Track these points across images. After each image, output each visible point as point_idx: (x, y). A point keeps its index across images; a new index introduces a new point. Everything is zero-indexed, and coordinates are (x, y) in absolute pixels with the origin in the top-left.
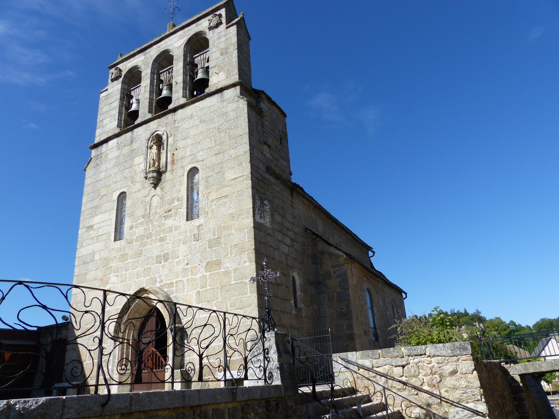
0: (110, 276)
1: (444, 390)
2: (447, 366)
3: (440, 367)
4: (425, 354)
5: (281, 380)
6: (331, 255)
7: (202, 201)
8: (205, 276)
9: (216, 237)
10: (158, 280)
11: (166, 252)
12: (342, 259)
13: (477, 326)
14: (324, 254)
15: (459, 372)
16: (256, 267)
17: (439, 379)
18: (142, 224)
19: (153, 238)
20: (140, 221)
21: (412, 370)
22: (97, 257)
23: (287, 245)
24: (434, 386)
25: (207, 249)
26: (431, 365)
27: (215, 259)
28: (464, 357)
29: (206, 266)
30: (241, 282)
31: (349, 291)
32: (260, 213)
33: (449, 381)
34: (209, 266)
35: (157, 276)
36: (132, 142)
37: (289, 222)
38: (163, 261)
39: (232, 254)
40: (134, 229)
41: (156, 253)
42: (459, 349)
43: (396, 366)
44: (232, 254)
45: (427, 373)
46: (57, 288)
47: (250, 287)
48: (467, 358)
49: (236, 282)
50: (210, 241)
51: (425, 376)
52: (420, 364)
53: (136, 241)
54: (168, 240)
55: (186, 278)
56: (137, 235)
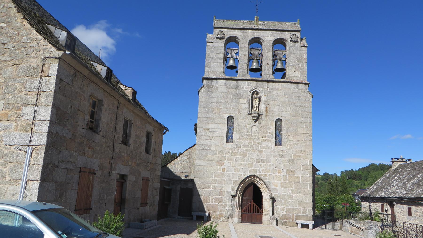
0: (225, 161)
18: (247, 139)
34: (288, 171)
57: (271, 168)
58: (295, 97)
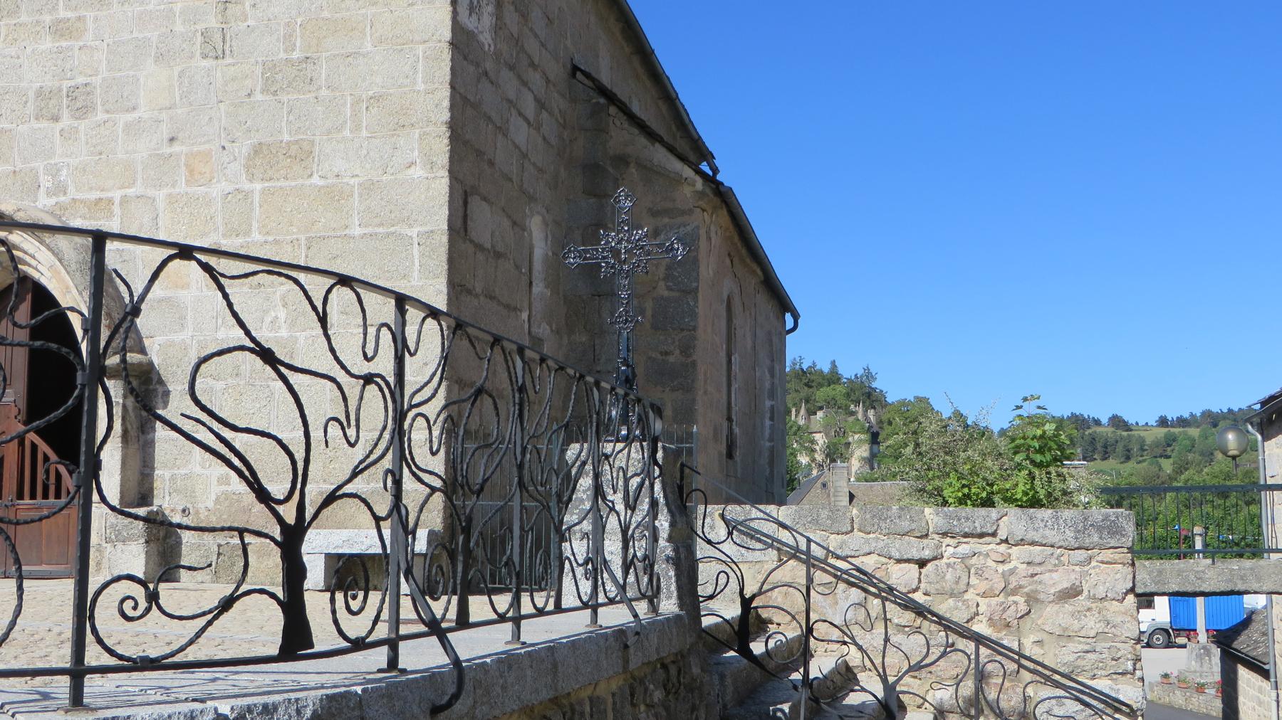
1: (1033, 638)
2: (1054, 575)
3: (1033, 576)
4: (994, 534)
5: (680, 597)
6: (650, 172)
8: (247, 195)
9: (296, 55)
10: (46, 181)
11: (80, 80)
12: (687, 190)
13: (860, 416)
14: (627, 164)
15: (1085, 593)
16: (451, 187)
17: (1023, 608)
19: (24, 18)
21: (948, 576)
24: (1008, 625)
25: (259, 97)
26: (1007, 567)
27: (286, 137)
28: (1108, 555)
29: (249, 158)
30: (388, 234)
31: (696, 299)
33: (1053, 616)
35: (40, 165)
37: (536, 36)
38: (65, 114)
42: (1100, 529)
43: (899, 561)
44: (357, 128)
45: (991, 589)
46: (296, 282)
47: (422, 255)
48: (1117, 557)
49: (369, 230)
51: (984, 595)
52: (974, 560)
55: (165, 191)
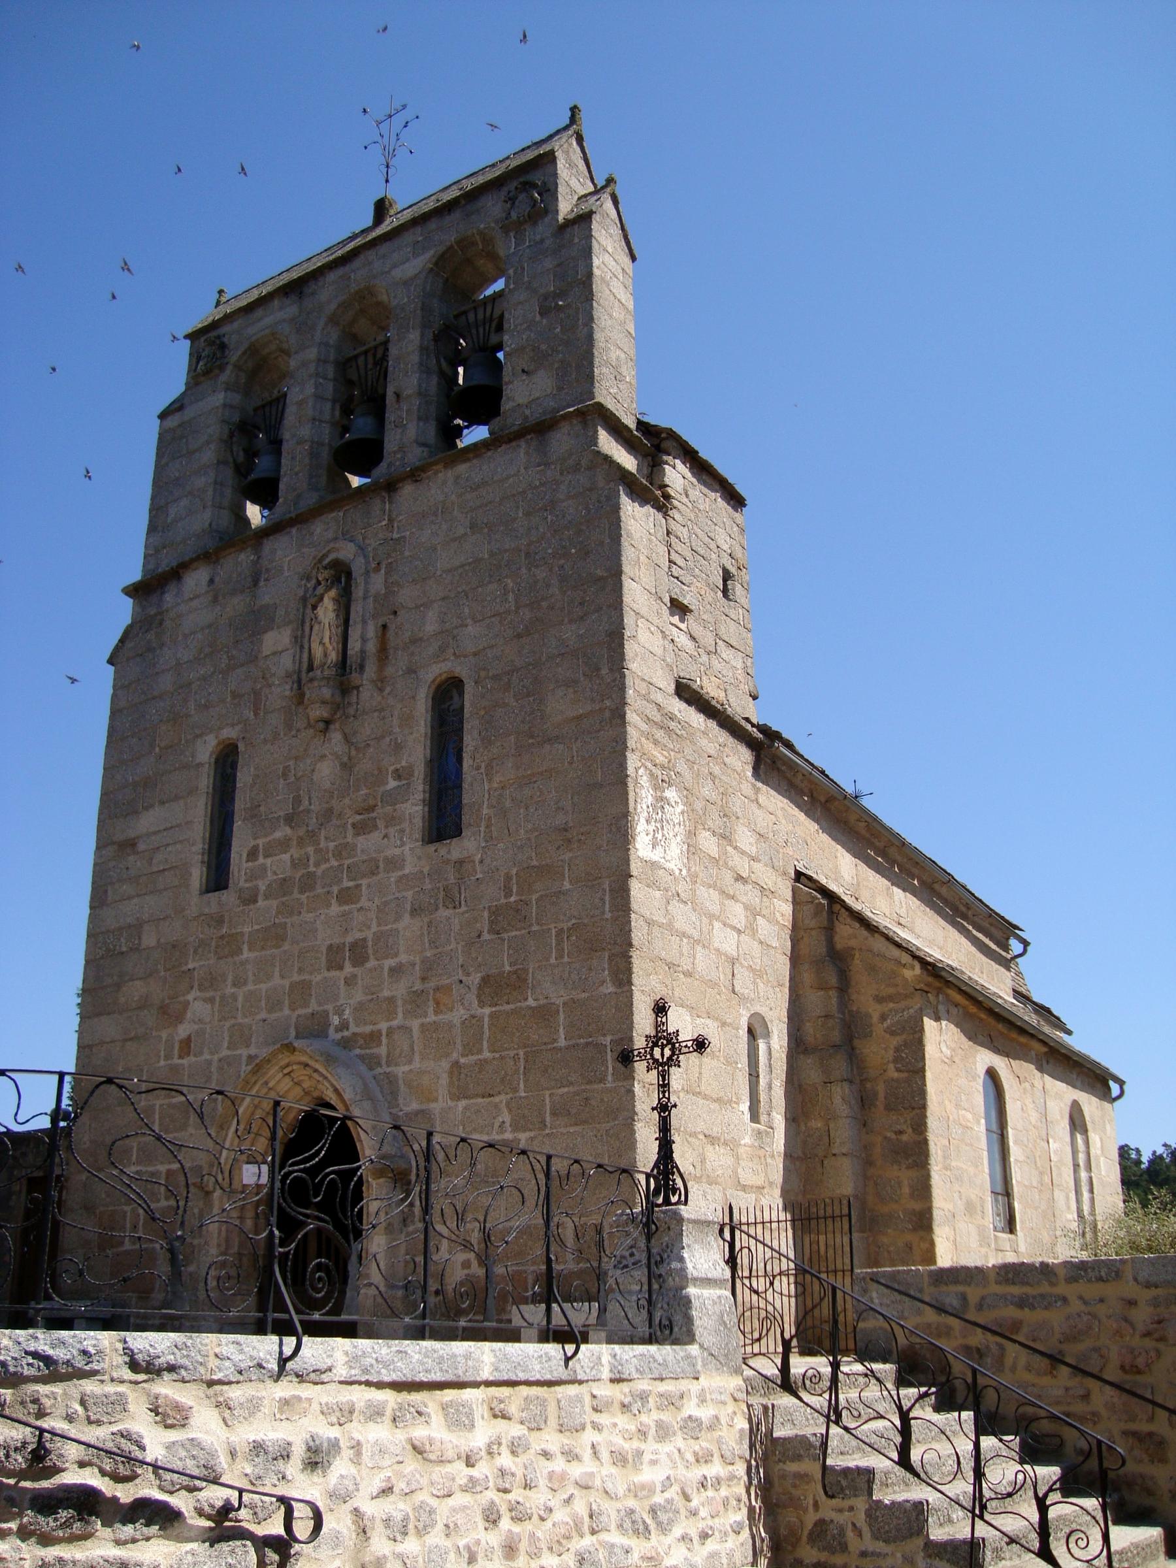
0: (190, 997)
7: (477, 788)
18: (284, 844)
20: (278, 834)
22: (149, 939)
23: (734, 928)
27: (507, 968)
29: (480, 988)
30: (587, 1044)
32: (651, 828)
34: (494, 987)
35: (329, 1007)
36: (256, 583)
38: (347, 964)
39: (560, 956)
40: (261, 860)
41: (325, 937)
50: (495, 912)
53: (267, 897)
54: (363, 899)
56: (270, 877)
57: (400, 990)
58: (527, 514)
